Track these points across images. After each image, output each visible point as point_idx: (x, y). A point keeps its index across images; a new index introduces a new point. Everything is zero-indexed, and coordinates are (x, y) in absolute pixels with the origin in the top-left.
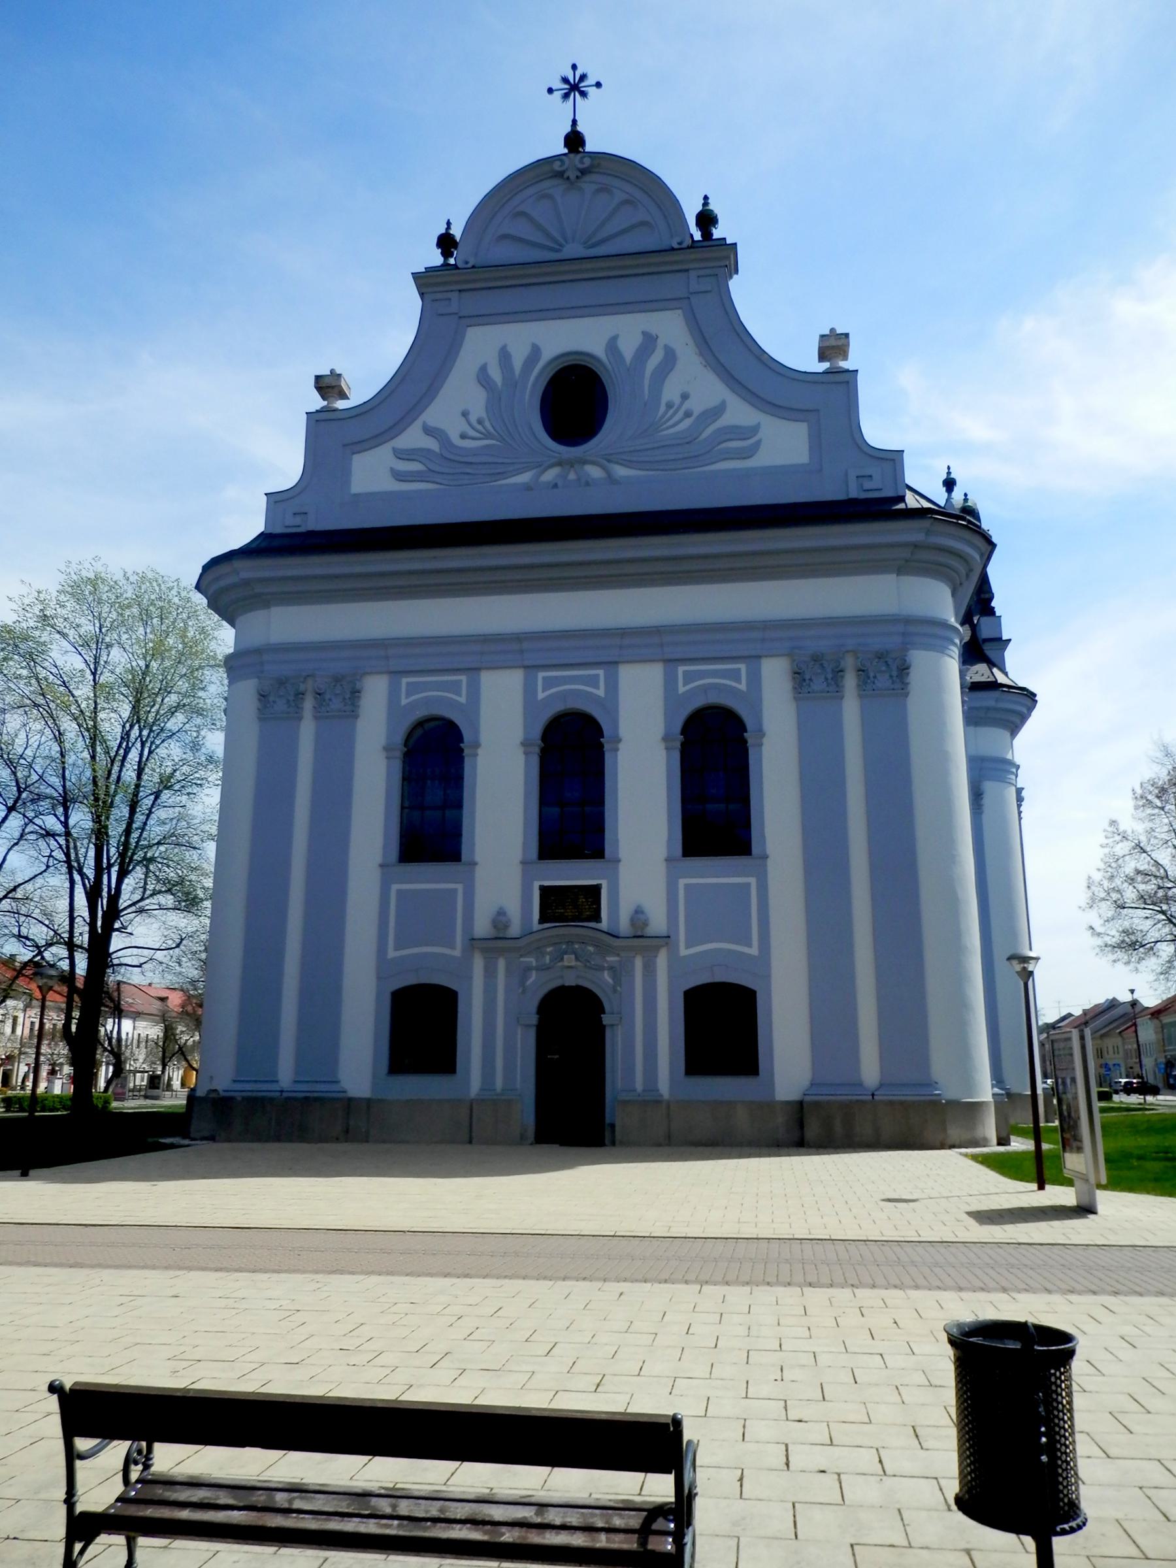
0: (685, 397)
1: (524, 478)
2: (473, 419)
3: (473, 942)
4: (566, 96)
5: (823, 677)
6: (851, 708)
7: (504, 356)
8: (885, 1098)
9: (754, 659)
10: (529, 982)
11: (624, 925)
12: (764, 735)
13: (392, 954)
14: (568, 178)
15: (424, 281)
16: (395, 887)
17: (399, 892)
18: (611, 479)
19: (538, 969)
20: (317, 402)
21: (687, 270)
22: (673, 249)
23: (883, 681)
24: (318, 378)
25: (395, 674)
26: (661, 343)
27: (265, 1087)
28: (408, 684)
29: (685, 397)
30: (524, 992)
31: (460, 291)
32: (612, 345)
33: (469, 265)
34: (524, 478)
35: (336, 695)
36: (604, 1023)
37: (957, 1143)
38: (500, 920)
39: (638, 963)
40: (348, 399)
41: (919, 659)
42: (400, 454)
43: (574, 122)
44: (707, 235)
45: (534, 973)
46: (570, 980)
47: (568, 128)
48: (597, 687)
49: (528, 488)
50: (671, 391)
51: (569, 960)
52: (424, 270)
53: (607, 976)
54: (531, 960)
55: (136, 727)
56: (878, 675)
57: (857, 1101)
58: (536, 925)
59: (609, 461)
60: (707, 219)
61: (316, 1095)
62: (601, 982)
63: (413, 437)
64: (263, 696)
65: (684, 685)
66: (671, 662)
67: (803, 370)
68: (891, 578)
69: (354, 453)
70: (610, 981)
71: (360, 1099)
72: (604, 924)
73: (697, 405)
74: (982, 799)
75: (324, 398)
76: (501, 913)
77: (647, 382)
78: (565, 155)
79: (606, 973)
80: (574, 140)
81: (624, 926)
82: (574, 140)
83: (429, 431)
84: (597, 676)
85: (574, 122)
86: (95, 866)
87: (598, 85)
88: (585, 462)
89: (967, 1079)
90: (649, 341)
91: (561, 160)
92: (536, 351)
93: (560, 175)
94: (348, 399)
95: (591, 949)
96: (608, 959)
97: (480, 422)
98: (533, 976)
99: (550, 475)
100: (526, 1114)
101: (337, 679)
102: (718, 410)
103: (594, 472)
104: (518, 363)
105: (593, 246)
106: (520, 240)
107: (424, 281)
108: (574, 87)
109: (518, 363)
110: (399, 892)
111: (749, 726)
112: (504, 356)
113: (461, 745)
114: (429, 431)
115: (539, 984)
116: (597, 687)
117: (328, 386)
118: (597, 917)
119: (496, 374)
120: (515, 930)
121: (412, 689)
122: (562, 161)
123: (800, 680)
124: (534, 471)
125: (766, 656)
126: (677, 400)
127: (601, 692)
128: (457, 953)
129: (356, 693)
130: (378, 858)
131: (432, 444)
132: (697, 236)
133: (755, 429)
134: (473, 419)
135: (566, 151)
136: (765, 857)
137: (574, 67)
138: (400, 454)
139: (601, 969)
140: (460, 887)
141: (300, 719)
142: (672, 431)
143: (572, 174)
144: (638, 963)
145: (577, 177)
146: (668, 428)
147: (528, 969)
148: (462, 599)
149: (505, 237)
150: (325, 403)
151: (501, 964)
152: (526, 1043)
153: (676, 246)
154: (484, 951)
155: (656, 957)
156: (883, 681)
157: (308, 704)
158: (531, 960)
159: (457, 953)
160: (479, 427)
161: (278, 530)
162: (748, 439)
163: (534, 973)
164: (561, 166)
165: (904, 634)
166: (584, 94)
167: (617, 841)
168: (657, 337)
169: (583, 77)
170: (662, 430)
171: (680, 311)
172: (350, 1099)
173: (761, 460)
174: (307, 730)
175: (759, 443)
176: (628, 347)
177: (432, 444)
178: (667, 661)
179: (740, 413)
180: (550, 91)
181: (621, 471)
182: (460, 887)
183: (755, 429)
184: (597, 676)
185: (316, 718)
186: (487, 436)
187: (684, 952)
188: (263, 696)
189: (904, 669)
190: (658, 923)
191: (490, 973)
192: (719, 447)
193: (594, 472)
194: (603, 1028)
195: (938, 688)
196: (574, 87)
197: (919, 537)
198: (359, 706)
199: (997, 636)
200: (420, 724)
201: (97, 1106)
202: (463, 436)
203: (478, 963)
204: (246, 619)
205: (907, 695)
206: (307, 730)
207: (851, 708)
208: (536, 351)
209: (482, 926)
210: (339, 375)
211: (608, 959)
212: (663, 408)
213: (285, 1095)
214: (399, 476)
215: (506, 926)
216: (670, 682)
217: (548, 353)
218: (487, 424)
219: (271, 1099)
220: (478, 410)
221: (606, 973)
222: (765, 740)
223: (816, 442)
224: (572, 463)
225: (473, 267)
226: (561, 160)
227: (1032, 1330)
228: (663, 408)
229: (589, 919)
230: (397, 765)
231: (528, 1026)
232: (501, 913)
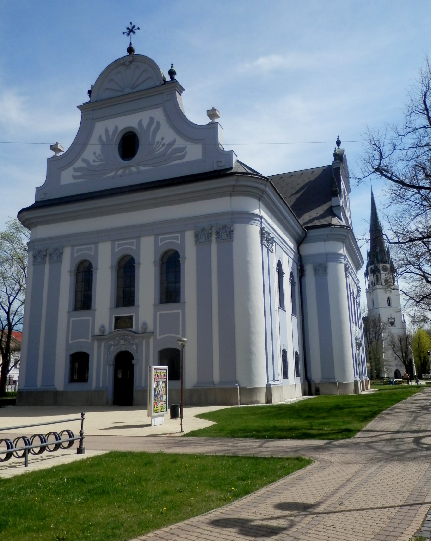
0: (163, 139)
1: (112, 174)
2: (97, 155)
3: (94, 336)
4: (128, 34)
5: (226, 234)
7: (107, 131)
8: (219, 387)
10: (111, 350)
12: (186, 259)
13: (70, 342)
14: (126, 65)
15: (83, 108)
16: (72, 319)
17: (160, 314)
18: (139, 172)
19: (114, 345)
20: (52, 153)
21: (163, 93)
22: (158, 86)
23: (224, 236)
24: (51, 146)
25: (73, 246)
26: (155, 120)
27: (32, 388)
28: (117, 244)
29: (163, 139)
30: (109, 353)
31: (93, 110)
32: (140, 123)
33: (94, 101)
34: (112, 174)
35: (223, 233)
36: (133, 363)
37: (245, 403)
39: (144, 342)
40: (219, 118)
43: (131, 43)
44: (172, 78)
45: (113, 347)
46: (123, 349)
47: (128, 46)
48: (133, 246)
49: (113, 177)
50: (158, 138)
51: (122, 342)
52: (82, 104)
53: (135, 347)
54: (112, 342)
56: (223, 234)
57: (210, 388)
58: (113, 330)
59: (138, 165)
60: (172, 73)
61: (46, 390)
62: (132, 349)
63: (79, 164)
64: (217, 233)
65: (117, 248)
67: (200, 125)
68: (228, 198)
69: (61, 171)
70: (136, 349)
71: (60, 391)
72: (134, 329)
73: (166, 141)
74: (327, 270)
75: (211, 119)
76: (103, 327)
77: (151, 134)
78: (128, 55)
79: (134, 346)
80: (130, 50)
81: (140, 330)
82: (130, 50)
83: (84, 161)
84: (133, 242)
85: (131, 43)
87: (138, 28)
88: (131, 166)
90: (152, 120)
91: (123, 59)
92: (116, 127)
93: (123, 64)
94: (219, 118)
95: (130, 338)
96: (135, 341)
97: (99, 156)
98: (112, 348)
99: (120, 172)
100: (110, 395)
101: (56, 249)
102: (172, 143)
103: (134, 169)
104: (111, 133)
105: (134, 88)
106: (112, 89)
107: (83, 108)
108: (131, 31)
109: (111, 133)
110: (160, 314)
111: (136, 261)
112: (107, 131)
113: (179, 259)
114: (84, 161)
115: (114, 351)
116: (133, 246)
117: (54, 148)
118: (131, 326)
119: (104, 138)
120: (107, 332)
121: (119, 245)
122: (124, 60)
124: (114, 172)
125: (187, 230)
126: (160, 140)
127: (134, 248)
128: (89, 341)
129: (61, 254)
130: (67, 310)
131: (84, 165)
132: (168, 78)
133: (184, 148)
134: (97, 155)
135: (128, 54)
136: (185, 302)
137: (131, 23)
138: (76, 170)
139: (133, 344)
140: (180, 311)
141: (45, 264)
142: (158, 152)
143: (127, 63)
144: (144, 342)
145: (129, 64)
146: (157, 151)
147: (111, 345)
148: (141, 211)
149: (107, 89)
150: (211, 121)
151: (103, 344)
152: (110, 370)
153: (159, 85)
154: (98, 340)
155: (150, 340)
156: (224, 236)
157: (214, 237)
158: (112, 342)
159: (89, 341)
160: (99, 158)
161: (39, 200)
162: (182, 152)
163: (113, 347)
164: (123, 61)
165: (232, 218)
166: (134, 33)
167: (185, 296)
168: (154, 118)
169: (134, 27)
170: (155, 152)
171: (161, 108)
172: (57, 392)
173: (187, 159)
175: (186, 152)
176: (145, 124)
177: (84, 165)
178: (155, 235)
179: (180, 142)
180: (124, 33)
181: (142, 168)
182: (180, 311)
183: (184, 148)
184: (133, 242)
185: (49, 263)
186: (101, 160)
187: (158, 337)
190: (150, 328)
191: (99, 347)
192: (174, 156)
194: (133, 365)
196: (131, 31)
197: (234, 183)
198: (233, 237)
199: (338, 205)
200: (166, 253)
202: (94, 161)
203: (96, 344)
204: (34, 229)
205: (232, 241)
206: (214, 247)
208: (116, 127)
210: (216, 109)
211: (135, 341)
212: (156, 144)
213: (38, 390)
214: (75, 177)
215: (103, 332)
217: (120, 128)
218: (101, 156)
219: (33, 392)
220: (98, 152)
221: (134, 346)
222: (186, 261)
223: (204, 152)
224: (125, 168)
225: (96, 101)
226: (123, 59)
228: (156, 144)
229: (129, 327)
230: (158, 268)
231: (110, 365)
232: (103, 327)
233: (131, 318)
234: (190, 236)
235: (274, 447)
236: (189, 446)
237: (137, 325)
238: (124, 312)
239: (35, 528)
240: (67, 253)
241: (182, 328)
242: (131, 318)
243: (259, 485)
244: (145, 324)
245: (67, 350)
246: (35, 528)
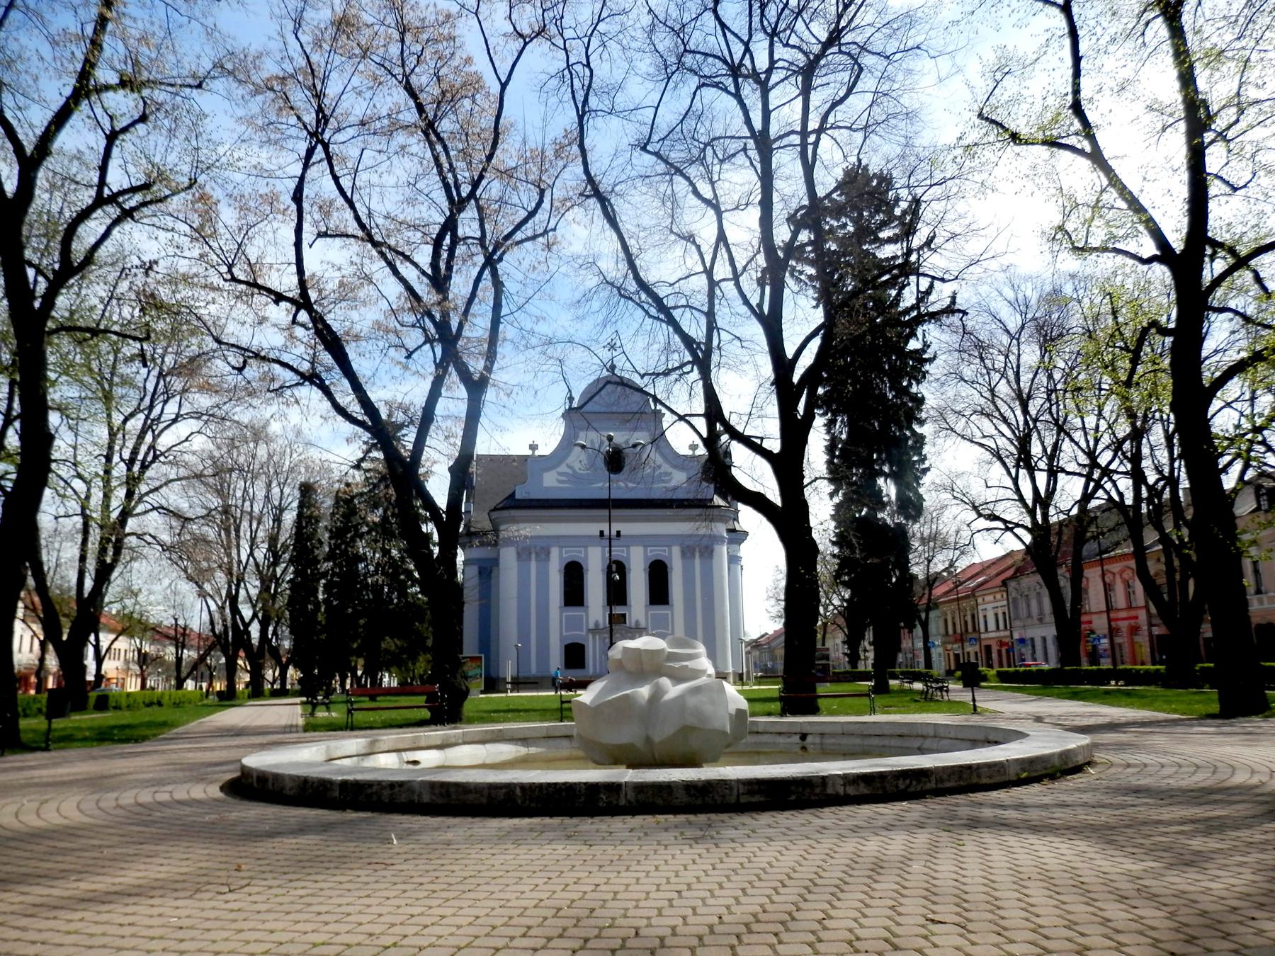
6: (697, 561)
9: (670, 546)
11: (633, 625)
25: (561, 547)
38: (597, 624)
41: (716, 547)
42: (559, 474)
55: (141, 416)
63: (563, 468)
66: (645, 547)
83: (568, 466)
86: (43, 483)
89: (726, 667)
101: (542, 548)
103: (622, 484)
123: (683, 554)
129: (549, 553)
131: (569, 471)
138: (559, 474)
174: (533, 564)
177: (569, 471)
188: (518, 554)
189: (712, 551)
190: (643, 624)
191: (594, 638)
193: (622, 484)
195: (721, 555)
201: (295, 667)
203: (591, 636)
207: (697, 561)
209: (591, 626)
216: (645, 551)
227: (518, 791)
233: (624, 615)
234: (676, 551)
235: (40, 777)
236: (1128, 694)
237: (630, 621)
238: (618, 610)
239: (825, 375)
240: (555, 552)
241: (694, 609)
242: (624, 615)
243: (731, 789)
244: (637, 622)
245: (561, 640)
246: (825, 375)
